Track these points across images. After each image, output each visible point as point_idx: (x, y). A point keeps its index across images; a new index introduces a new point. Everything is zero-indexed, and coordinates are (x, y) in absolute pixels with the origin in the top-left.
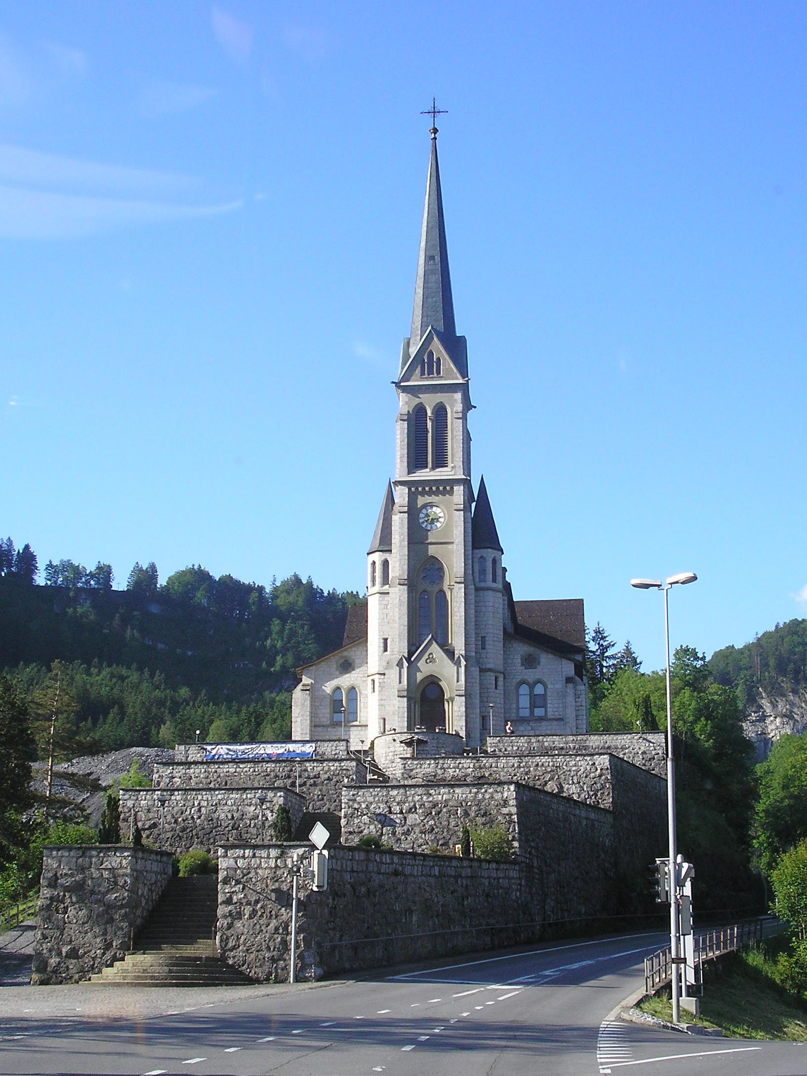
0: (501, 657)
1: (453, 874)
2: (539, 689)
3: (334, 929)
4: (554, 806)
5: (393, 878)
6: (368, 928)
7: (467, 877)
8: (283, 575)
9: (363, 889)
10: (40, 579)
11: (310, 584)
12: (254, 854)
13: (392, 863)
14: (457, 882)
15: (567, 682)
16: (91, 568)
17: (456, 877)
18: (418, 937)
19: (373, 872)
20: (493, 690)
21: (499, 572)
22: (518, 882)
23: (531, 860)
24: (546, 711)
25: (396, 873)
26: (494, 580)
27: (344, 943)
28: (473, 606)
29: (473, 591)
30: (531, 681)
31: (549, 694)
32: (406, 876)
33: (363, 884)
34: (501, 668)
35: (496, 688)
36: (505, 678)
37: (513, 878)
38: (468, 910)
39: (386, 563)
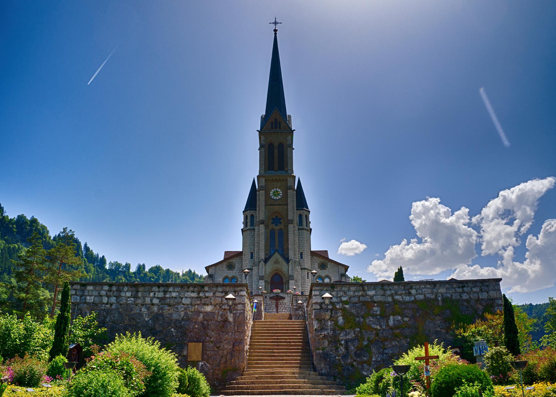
10: (107, 267)
11: (194, 273)
12: (460, 296)
16: (124, 264)
28: (297, 236)
30: (323, 276)
39: (252, 216)
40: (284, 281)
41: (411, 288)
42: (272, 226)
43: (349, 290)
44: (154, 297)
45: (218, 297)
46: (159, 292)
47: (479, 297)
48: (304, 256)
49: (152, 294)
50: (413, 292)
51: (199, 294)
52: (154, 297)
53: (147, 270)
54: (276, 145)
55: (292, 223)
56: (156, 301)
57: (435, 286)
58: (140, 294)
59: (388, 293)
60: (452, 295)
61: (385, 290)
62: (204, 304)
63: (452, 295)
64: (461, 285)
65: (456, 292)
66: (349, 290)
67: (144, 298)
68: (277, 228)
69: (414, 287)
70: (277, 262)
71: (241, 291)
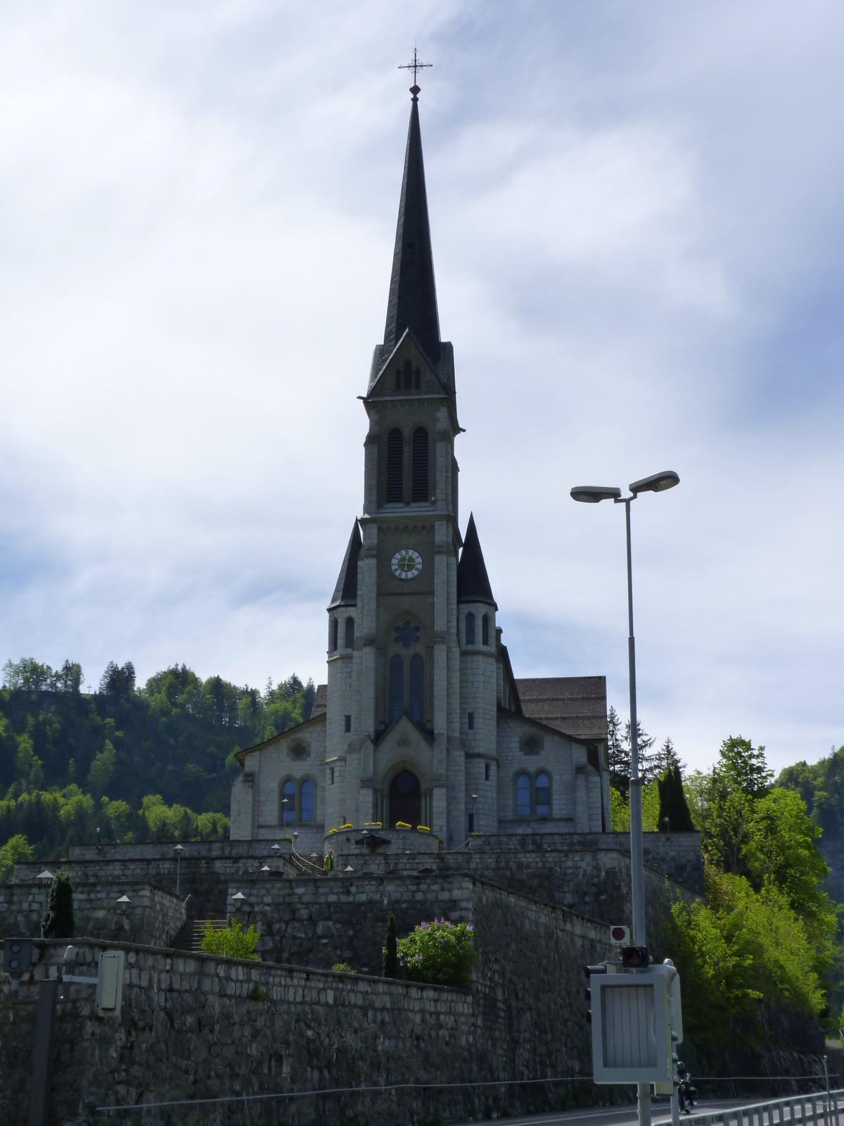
0: (494, 739)
1: (360, 1002)
2: (542, 782)
3: (127, 1083)
4: (532, 915)
5: (251, 1005)
6: (195, 1082)
7: (383, 1009)
8: (281, 678)
9: (190, 1020)
13: (249, 980)
14: (365, 1015)
15: (576, 773)
16: (57, 667)
17: (364, 1010)
18: (291, 1098)
19: (212, 992)
20: (482, 781)
21: (492, 633)
22: (472, 1020)
23: (493, 989)
24: (551, 809)
25: (254, 996)
26: (485, 642)
27: (145, 1106)
28: (457, 674)
29: (458, 655)
31: (555, 787)
32: (273, 1002)
33: (190, 1011)
34: (494, 753)
35: (487, 779)
36: (498, 766)
37: (462, 1014)
38: (383, 1060)
40: (423, 787)
41: (352, 885)
42: (395, 649)
43: (273, 887)
44: (34, 901)
45: (112, 898)
46: (39, 894)
47: (437, 898)
48: (478, 722)
49: (30, 898)
50: (353, 889)
51: (89, 895)
52: (34, 901)
53: (140, 683)
54: (407, 432)
55: (442, 642)
56: (35, 906)
57: (382, 882)
58: (15, 899)
59: (321, 890)
60: (402, 895)
61: (317, 888)
62: (95, 909)
63: (402, 895)
64: (416, 881)
65: (408, 890)
66: (273, 887)
67: (21, 902)
68: (406, 653)
69: (355, 883)
70: (404, 742)
71: (141, 889)
